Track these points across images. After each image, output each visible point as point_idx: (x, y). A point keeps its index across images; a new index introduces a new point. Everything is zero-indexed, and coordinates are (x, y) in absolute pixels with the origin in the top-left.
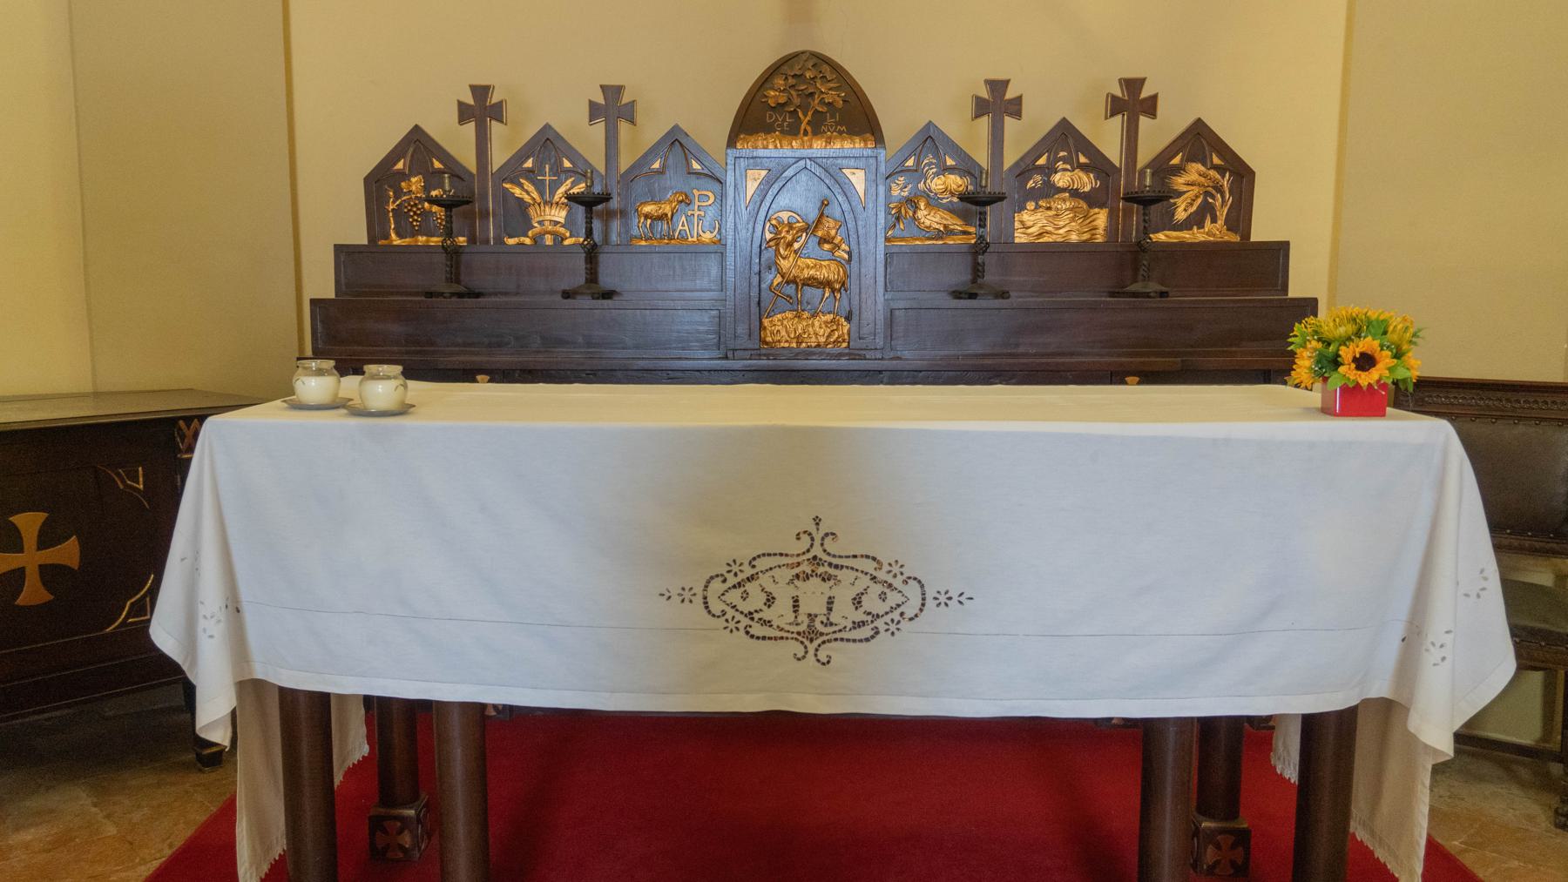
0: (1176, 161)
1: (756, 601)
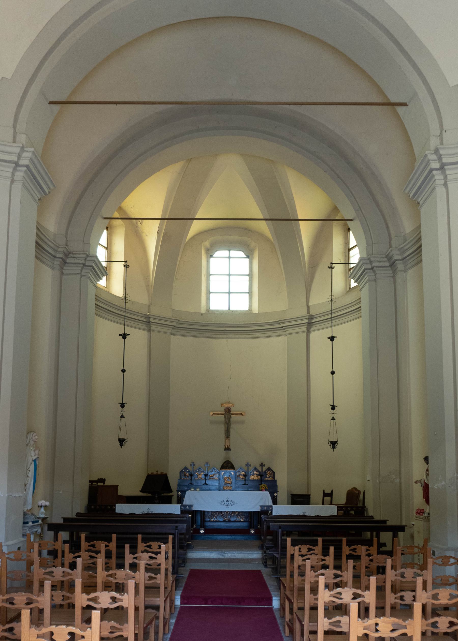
0: (267, 471)
1: (224, 503)
